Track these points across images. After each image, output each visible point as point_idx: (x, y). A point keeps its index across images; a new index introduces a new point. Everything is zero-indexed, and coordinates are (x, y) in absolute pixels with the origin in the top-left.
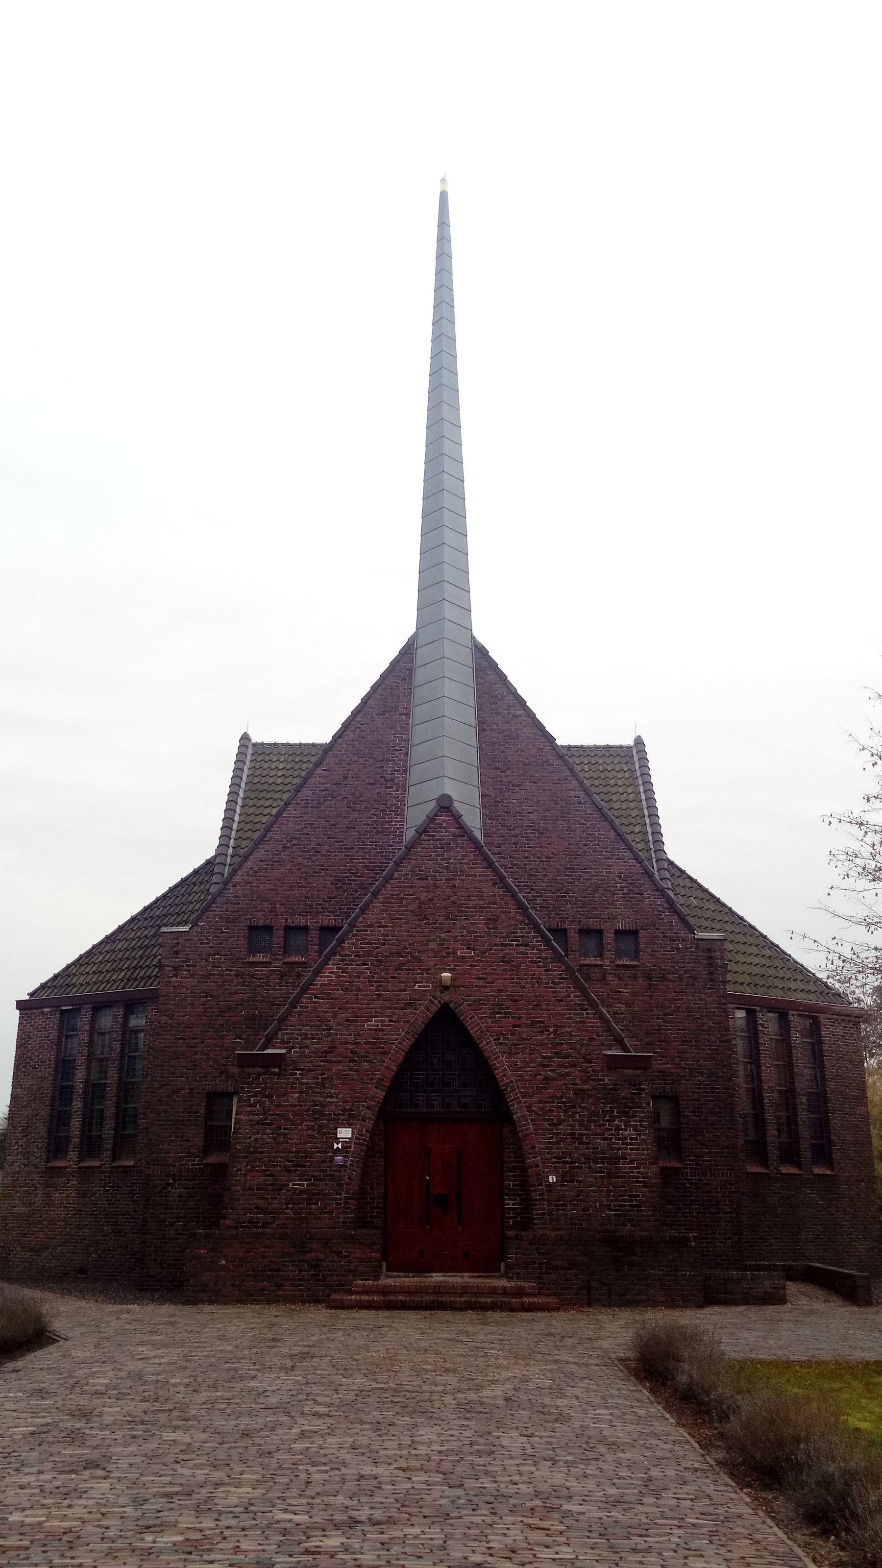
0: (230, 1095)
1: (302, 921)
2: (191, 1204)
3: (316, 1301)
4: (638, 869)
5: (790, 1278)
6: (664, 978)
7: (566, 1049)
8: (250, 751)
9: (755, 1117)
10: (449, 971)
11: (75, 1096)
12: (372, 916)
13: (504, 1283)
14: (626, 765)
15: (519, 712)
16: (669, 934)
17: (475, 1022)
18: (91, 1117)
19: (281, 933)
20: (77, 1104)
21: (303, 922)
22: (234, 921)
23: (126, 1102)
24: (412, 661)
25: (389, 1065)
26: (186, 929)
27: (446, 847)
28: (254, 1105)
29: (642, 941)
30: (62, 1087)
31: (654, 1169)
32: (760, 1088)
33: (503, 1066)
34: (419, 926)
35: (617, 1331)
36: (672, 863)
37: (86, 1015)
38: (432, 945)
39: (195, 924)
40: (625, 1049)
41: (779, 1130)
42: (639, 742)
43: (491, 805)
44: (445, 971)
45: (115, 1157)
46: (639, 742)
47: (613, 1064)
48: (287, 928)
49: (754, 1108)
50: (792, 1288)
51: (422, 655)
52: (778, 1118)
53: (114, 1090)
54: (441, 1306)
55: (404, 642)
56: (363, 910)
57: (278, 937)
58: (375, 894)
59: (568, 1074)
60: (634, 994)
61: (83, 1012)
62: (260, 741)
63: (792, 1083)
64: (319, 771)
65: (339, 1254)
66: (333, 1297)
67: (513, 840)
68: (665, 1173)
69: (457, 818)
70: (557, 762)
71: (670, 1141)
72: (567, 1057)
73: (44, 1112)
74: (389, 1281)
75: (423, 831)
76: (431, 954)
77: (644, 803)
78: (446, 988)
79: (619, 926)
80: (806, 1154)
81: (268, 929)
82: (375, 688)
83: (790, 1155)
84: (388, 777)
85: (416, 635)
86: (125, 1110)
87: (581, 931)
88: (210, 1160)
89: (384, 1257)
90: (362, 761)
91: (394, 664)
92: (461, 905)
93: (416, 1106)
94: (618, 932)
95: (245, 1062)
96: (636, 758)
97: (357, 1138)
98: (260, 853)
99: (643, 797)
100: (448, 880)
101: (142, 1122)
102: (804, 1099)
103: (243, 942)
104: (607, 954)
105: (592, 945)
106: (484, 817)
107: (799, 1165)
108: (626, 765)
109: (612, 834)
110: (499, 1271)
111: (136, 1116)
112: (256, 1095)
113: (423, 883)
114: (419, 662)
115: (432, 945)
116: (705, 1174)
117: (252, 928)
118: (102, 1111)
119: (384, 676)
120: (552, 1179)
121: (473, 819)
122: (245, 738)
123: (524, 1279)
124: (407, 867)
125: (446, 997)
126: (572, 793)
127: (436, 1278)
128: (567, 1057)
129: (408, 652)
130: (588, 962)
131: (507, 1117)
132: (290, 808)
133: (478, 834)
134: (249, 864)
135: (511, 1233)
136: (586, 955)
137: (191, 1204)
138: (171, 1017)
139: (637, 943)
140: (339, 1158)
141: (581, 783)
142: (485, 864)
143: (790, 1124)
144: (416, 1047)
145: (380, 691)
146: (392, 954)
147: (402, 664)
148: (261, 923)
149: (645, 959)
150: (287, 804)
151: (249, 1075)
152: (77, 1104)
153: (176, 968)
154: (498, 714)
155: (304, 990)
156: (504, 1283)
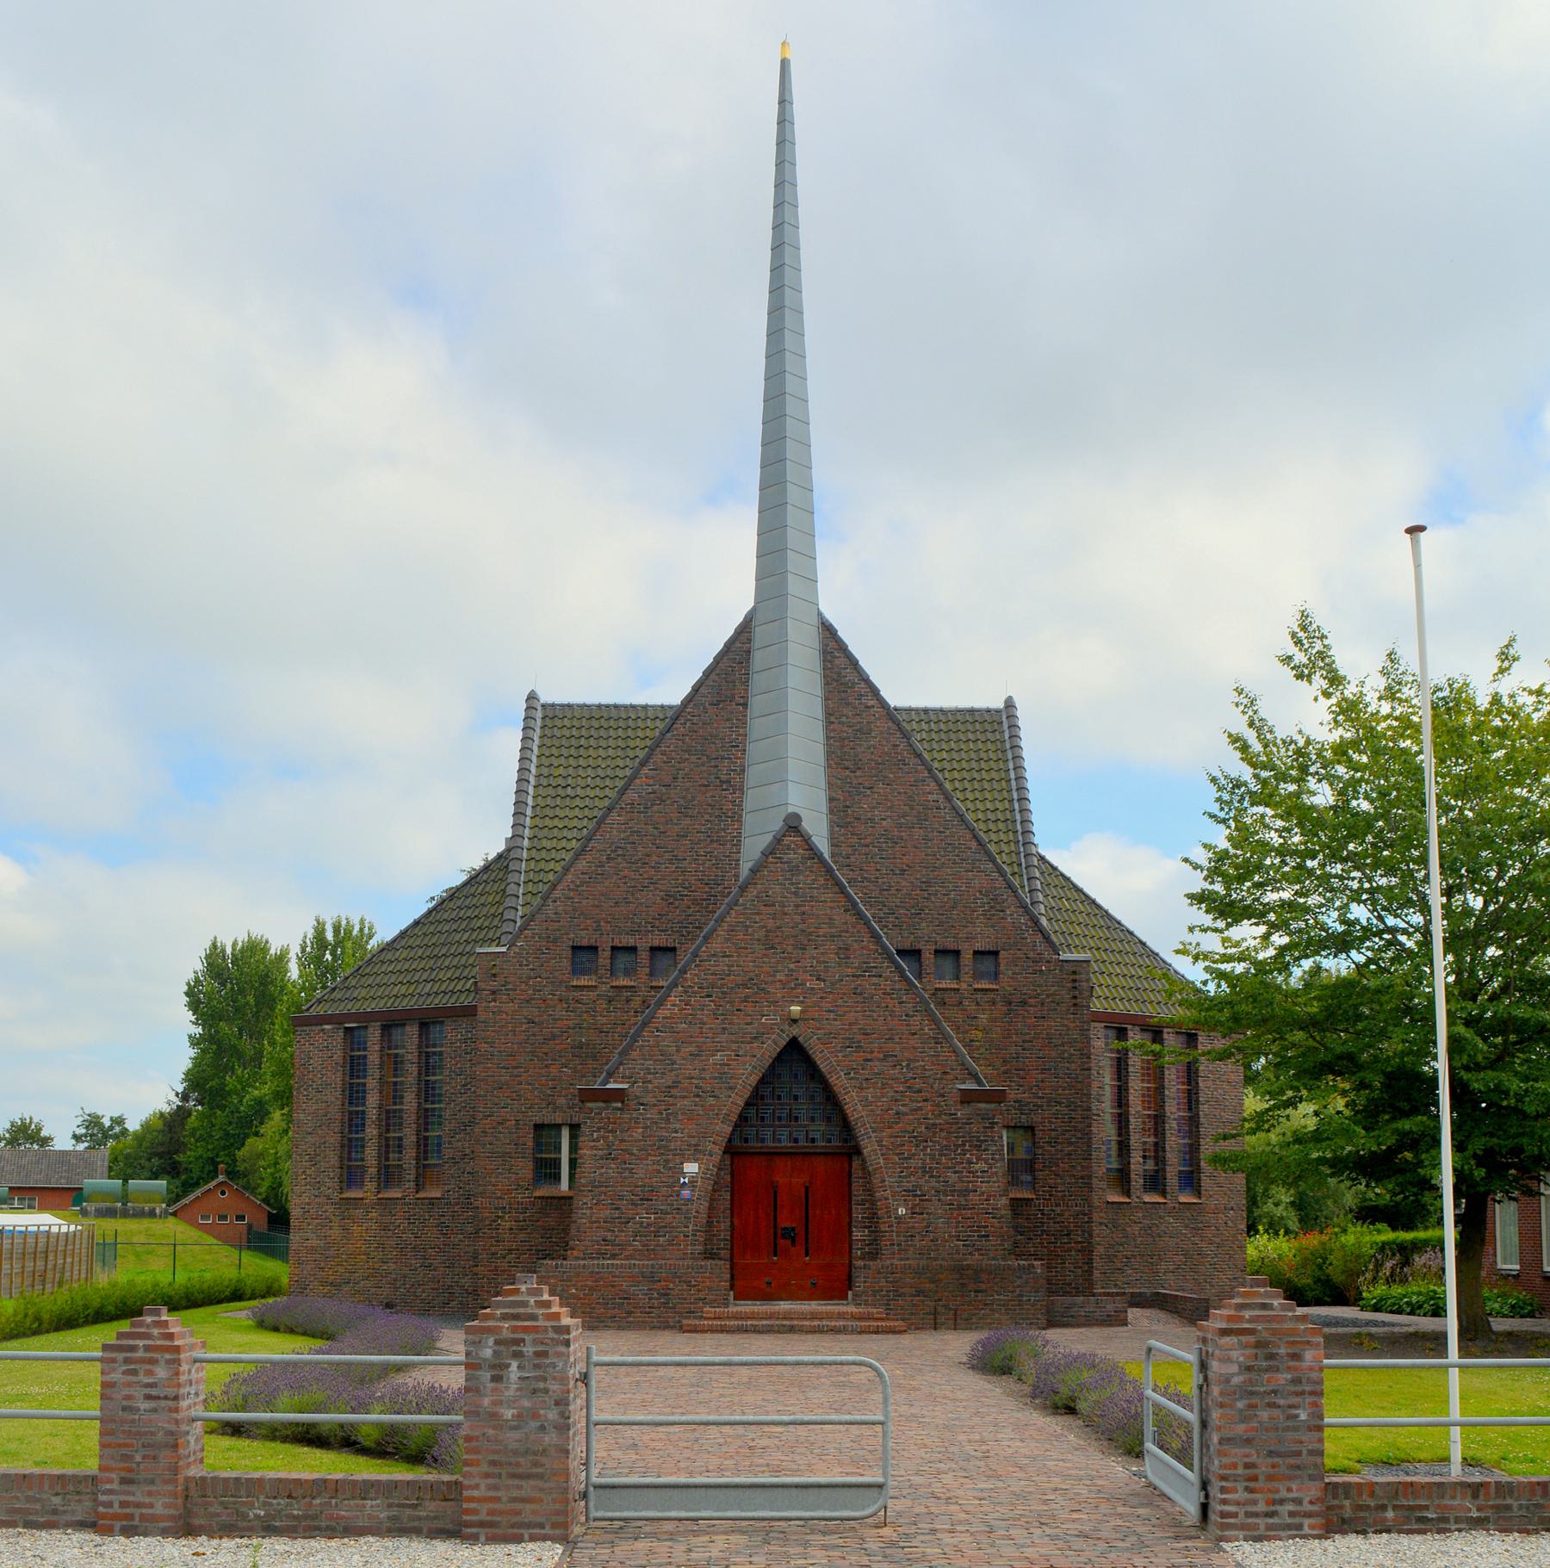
0: (558, 1127)
1: (629, 941)
2: (522, 1236)
3: (672, 1328)
4: (1000, 883)
5: (1132, 1305)
6: (1024, 1003)
7: (918, 1084)
8: (539, 714)
9: (1120, 1143)
10: (800, 1003)
11: (368, 1122)
12: (716, 945)
13: (851, 1309)
14: (990, 735)
15: (871, 703)
16: (1031, 955)
17: (824, 1059)
18: (387, 1146)
19: (608, 953)
20: (371, 1131)
21: (631, 942)
22: (555, 941)
23: (427, 1130)
24: (749, 640)
25: (736, 1101)
26: (504, 949)
27: (795, 870)
28: (597, 1140)
29: (1003, 962)
30: (351, 1113)
31: (1004, 1201)
32: (1127, 1113)
33: (855, 1104)
34: (765, 956)
35: (960, 1344)
36: (1042, 858)
37: (374, 1034)
38: (779, 976)
39: (512, 945)
40: (979, 1082)
41: (1144, 1157)
42: (1010, 704)
43: (840, 812)
44: (792, 1003)
45: (419, 1187)
46: (1010, 704)
47: (967, 1098)
48: (614, 948)
49: (1120, 1135)
50: (1133, 1313)
51: (760, 634)
52: (1145, 1143)
53: (414, 1117)
54: (792, 1330)
55: (739, 619)
56: (706, 938)
57: (604, 956)
58: (721, 919)
59: (920, 1109)
60: (993, 1020)
61: (371, 1030)
62: (550, 701)
63: (1163, 1107)
64: (645, 770)
65: (688, 1283)
66: (685, 1322)
67: (864, 850)
68: (1016, 1203)
69: (807, 842)
70: (914, 761)
71: (1022, 1169)
72: (919, 1091)
73: (334, 1139)
74: (739, 1309)
75: (769, 852)
76: (778, 985)
77: (1013, 783)
78: (795, 1021)
79: (978, 946)
80: (1172, 1179)
81: (593, 949)
82: (708, 673)
83: (1155, 1182)
84: (724, 777)
85: (754, 610)
86: (426, 1138)
87: (936, 951)
88: (537, 1194)
89: (732, 1287)
90: (693, 759)
91: (729, 645)
92: (810, 934)
93: (763, 1140)
94: (976, 953)
95: (587, 1096)
96: (1005, 726)
97: (704, 1172)
98: (582, 864)
99: (1012, 775)
100: (797, 906)
101: (448, 1152)
102: (1174, 1124)
103: (566, 963)
104: (965, 978)
105: (948, 964)
106: (832, 824)
107: (1164, 1194)
108: (990, 735)
109: (974, 844)
110: (846, 1298)
111: (439, 1145)
112: (599, 1129)
113: (771, 910)
114: (757, 644)
115: (779, 976)
116: (1058, 1205)
117: (576, 949)
118: (400, 1139)
119: (718, 659)
120: (902, 1211)
121: (818, 829)
122: (532, 697)
123: (874, 1306)
124: (753, 892)
125: (795, 1031)
126: (930, 797)
127: (784, 1306)
128: (919, 1091)
129: (745, 631)
130: (943, 986)
131: (858, 1151)
132: (614, 814)
133: (827, 856)
134: (569, 877)
135: (861, 1263)
136: (942, 978)
137: (522, 1236)
138: (492, 1045)
139: (997, 965)
140: (686, 1193)
141: (940, 785)
142: (836, 889)
143: (1158, 1152)
144: (762, 1081)
145: (713, 676)
146: (738, 986)
147: (738, 645)
148: (585, 943)
149: (1005, 983)
150: (610, 809)
151: (591, 1110)
152: (371, 1131)
153: (494, 993)
154: (848, 704)
155: (645, 1024)
156: (851, 1309)
